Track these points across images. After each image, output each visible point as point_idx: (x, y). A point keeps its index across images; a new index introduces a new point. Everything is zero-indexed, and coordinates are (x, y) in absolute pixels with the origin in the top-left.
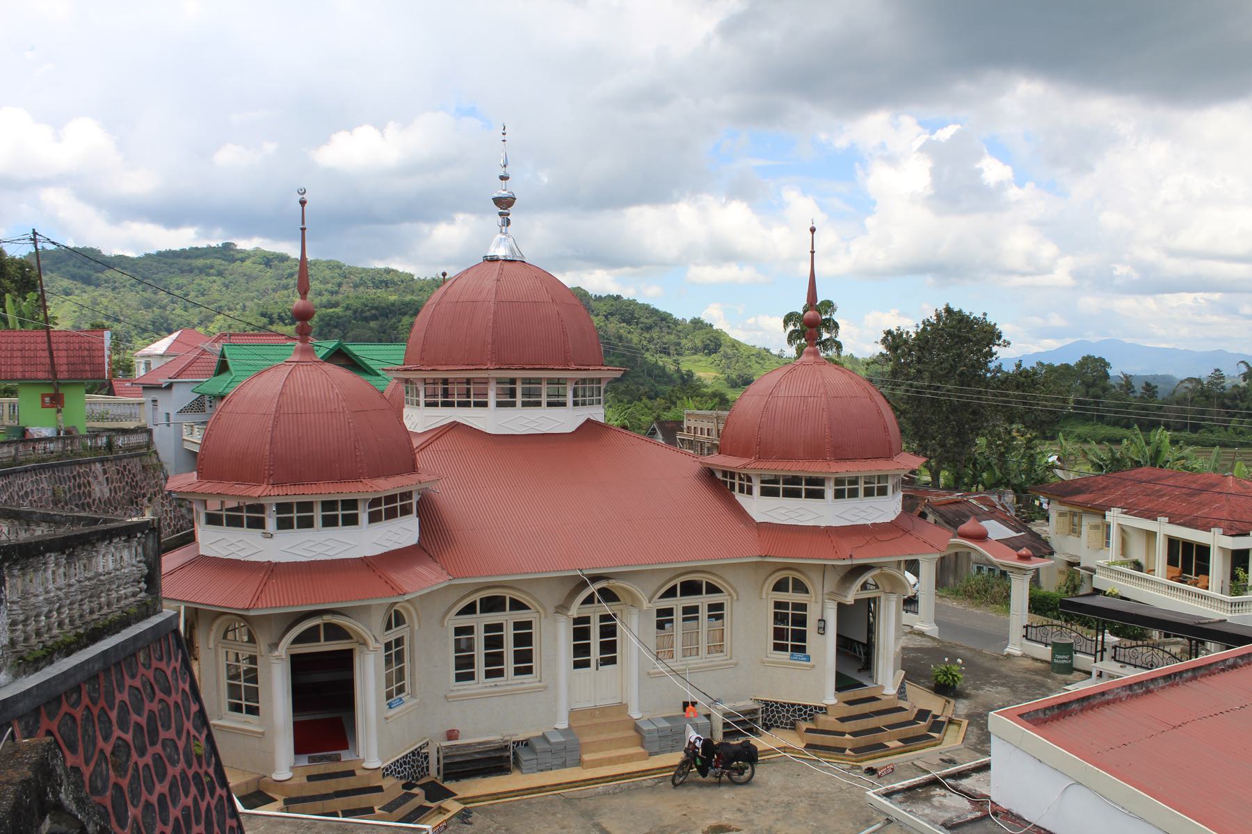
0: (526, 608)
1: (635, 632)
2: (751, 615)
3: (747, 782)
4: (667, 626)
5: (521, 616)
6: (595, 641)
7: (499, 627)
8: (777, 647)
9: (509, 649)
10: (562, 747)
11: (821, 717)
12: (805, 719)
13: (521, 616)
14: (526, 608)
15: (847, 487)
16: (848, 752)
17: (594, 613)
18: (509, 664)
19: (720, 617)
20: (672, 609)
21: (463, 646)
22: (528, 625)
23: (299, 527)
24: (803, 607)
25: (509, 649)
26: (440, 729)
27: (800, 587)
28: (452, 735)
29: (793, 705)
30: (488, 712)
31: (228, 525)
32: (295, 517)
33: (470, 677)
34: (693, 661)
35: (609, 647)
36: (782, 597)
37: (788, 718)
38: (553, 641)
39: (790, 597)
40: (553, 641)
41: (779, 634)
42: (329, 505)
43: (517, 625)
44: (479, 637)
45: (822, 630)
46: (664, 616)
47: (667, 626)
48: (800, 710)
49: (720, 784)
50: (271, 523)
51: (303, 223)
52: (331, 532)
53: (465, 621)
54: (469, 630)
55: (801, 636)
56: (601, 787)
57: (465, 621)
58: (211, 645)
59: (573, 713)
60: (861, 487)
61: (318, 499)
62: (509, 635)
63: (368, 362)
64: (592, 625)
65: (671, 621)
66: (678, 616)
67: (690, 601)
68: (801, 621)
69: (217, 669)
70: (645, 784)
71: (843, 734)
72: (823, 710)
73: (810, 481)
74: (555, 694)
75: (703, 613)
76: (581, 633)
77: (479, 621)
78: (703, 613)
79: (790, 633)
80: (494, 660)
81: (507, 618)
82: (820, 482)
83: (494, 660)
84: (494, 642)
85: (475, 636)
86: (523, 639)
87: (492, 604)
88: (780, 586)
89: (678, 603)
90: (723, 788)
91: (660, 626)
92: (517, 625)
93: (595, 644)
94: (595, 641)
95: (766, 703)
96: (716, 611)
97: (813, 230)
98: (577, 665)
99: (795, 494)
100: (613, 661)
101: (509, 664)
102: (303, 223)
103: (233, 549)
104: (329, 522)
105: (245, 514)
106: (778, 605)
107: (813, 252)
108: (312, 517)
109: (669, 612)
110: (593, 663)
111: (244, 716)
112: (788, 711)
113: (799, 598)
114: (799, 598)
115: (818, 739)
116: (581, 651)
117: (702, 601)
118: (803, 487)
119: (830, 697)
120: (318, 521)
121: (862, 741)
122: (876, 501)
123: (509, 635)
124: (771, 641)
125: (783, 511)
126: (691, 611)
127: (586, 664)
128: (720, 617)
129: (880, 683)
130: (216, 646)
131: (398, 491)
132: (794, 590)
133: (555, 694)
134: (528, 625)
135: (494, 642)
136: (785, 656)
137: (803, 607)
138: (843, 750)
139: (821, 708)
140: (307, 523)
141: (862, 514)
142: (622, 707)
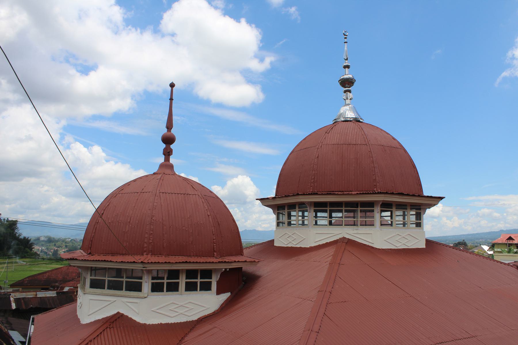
15: (199, 280)
42: (191, 274)
50: (146, 286)
51: (169, 126)
102: (169, 126)
108: (178, 283)
140: (173, 288)
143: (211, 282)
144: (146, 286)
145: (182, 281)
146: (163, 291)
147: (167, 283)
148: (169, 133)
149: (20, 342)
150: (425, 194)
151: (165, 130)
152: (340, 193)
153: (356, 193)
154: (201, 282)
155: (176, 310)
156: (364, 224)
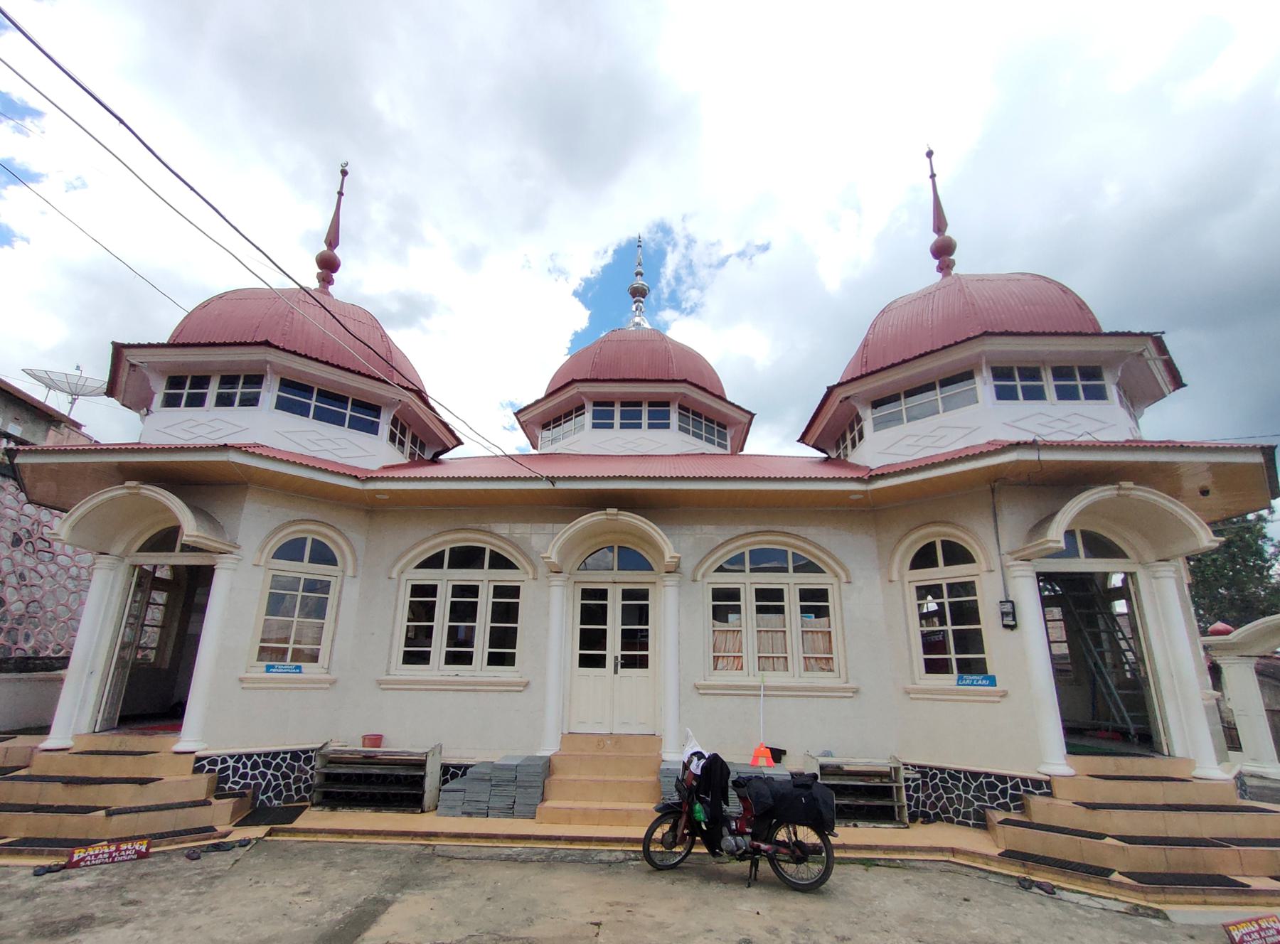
0: (515, 567)
1: (677, 618)
2: (876, 601)
3: (813, 888)
4: (732, 617)
5: (505, 577)
6: (614, 627)
7: (473, 591)
8: (934, 667)
9: (483, 624)
10: (511, 775)
11: (1037, 802)
12: (1005, 807)
13: (505, 577)
14: (515, 567)
16: (1115, 877)
17: (615, 583)
18: (481, 647)
19: (822, 612)
21: (461, 635)
22: (514, 591)
24: (968, 588)
27: (957, 554)
29: (976, 775)
30: (437, 716)
33: (423, 658)
34: (774, 678)
35: (636, 641)
36: (928, 576)
37: (969, 803)
38: (550, 621)
39: (943, 574)
40: (550, 621)
41: (932, 644)
43: (499, 591)
44: (443, 602)
45: (1010, 618)
46: (725, 604)
47: (732, 617)
48: (992, 786)
49: (751, 880)
53: (427, 577)
54: (431, 590)
55: (970, 641)
56: (519, 846)
57: (427, 577)
59: (569, 737)
62: (485, 603)
64: (609, 603)
65: (737, 610)
66: (748, 602)
67: (769, 580)
68: (966, 613)
70: (604, 857)
71: (1101, 836)
72: (1043, 786)
74: (542, 702)
75: (792, 603)
76: (593, 612)
77: (446, 580)
78: (792, 603)
79: (953, 642)
81: (484, 579)
84: (463, 611)
86: (506, 611)
87: (467, 557)
88: (924, 558)
89: (748, 583)
90: (753, 891)
91: (720, 614)
92: (499, 591)
93: (614, 634)
94: (614, 627)
95: (922, 770)
96: (815, 603)
97: (930, 154)
98: (586, 662)
100: (642, 662)
106: (923, 592)
107: (933, 176)
109: (734, 594)
110: (610, 662)
112: (966, 788)
113: (958, 573)
115: (1033, 842)
116: (592, 641)
117: (791, 584)
119: (1050, 756)
121: (1155, 859)
123: (485, 603)
124: (919, 657)
125: (911, 441)
126: (770, 601)
127: (599, 662)
128: (822, 612)
129: (1178, 751)
132: (948, 562)
133: (542, 702)
134: (514, 591)
135: (463, 611)
136: (947, 681)
137: (968, 588)
138: (1101, 873)
139: (1037, 784)
141: (1063, 426)
142: (653, 740)
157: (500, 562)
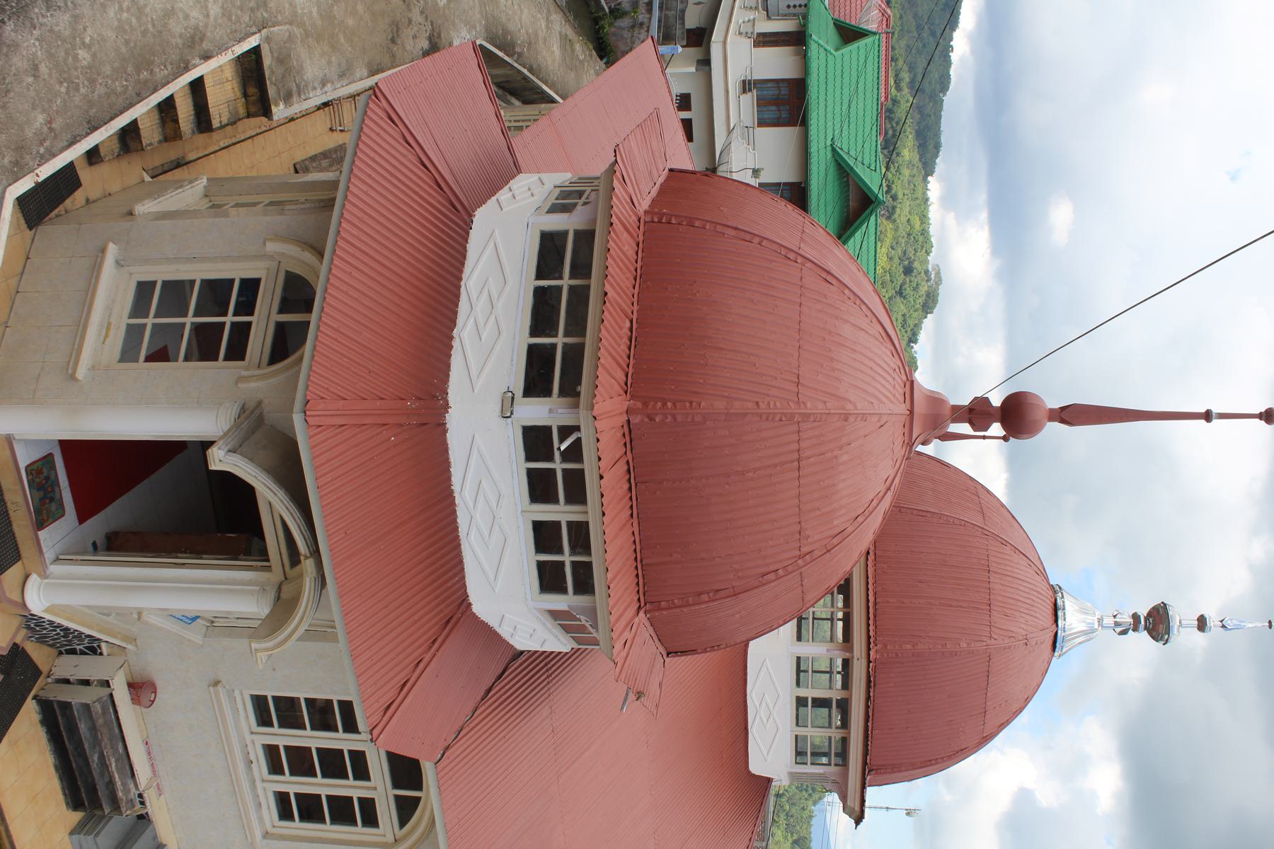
15: (567, 558)
20: (368, 778)
23: (530, 472)
25: (321, 786)
26: (156, 664)
28: (141, 689)
31: (532, 349)
32: (549, 466)
35: (310, 809)
42: (580, 534)
50: (538, 412)
51: (1072, 415)
52: (526, 538)
58: (272, 247)
60: (560, 513)
61: (590, 513)
62: (349, 788)
63: (858, 235)
69: (224, 259)
73: (574, 357)
76: (322, 714)
80: (300, 761)
81: (379, 787)
82: (570, 389)
83: (300, 761)
84: (333, 764)
85: (340, 734)
86: (342, 811)
99: (542, 317)
101: (295, 785)
102: (1072, 415)
103: (481, 305)
104: (545, 535)
105: (560, 340)
108: (556, 501)
111: (122, 319)
113: (260, 340)
114: (260, 340)
118: (560, 340)
120: (546, 512)
122: (521, 558)
123: (349, 788)
130: (270, 257)
131: (596, 558)
135: (333, 764)
137: (237, 351)
140: (540, 487)
143: (563, 590)
144: (538, 412)
145: (560, 513)
146: (529, 458)
147: (553, 471)
148: (1041, 415)
149: (403, 823)
150: (871, 792)
151: (1054, 403)
152: (871, 610)
153: (871, 633)
154: (562, 564)
155: (481, 499)
156: (809, 265)
157: (406, 809)
